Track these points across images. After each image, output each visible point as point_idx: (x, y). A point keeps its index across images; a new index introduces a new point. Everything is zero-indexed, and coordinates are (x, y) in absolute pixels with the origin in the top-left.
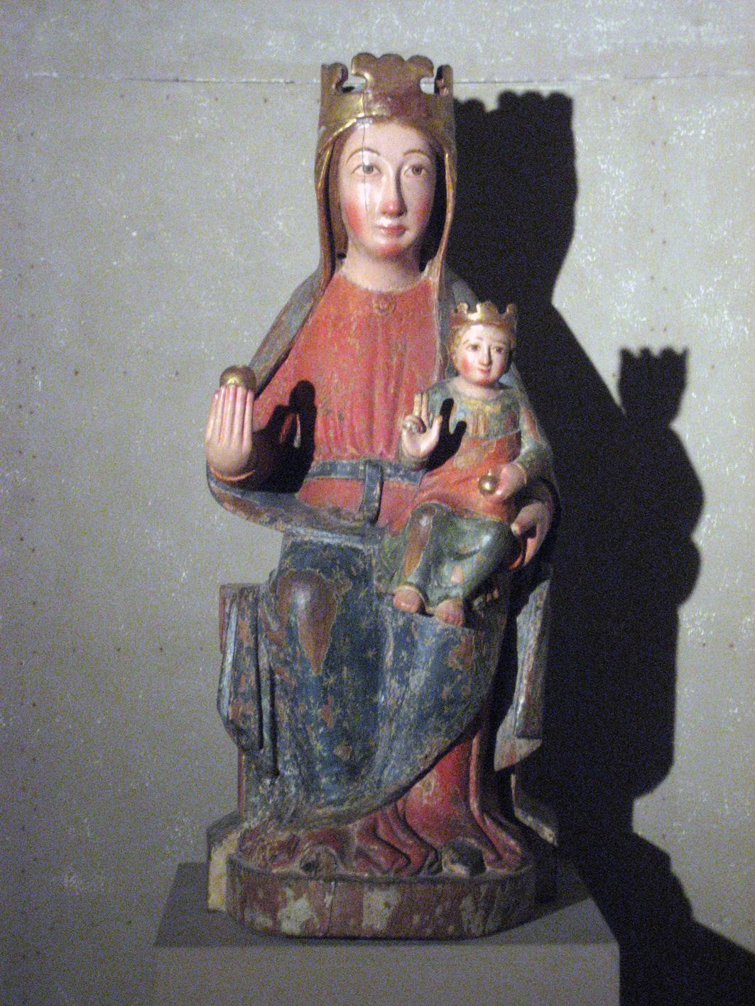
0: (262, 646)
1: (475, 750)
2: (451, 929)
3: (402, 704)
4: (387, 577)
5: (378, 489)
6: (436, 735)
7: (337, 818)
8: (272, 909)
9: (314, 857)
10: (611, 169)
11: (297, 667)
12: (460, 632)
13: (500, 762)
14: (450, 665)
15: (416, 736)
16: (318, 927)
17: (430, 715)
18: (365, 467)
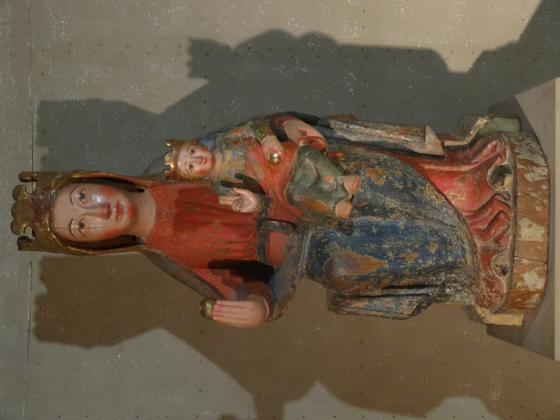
0: (368, 293)
1: (432, 167)
2: (544, 187)
3: (405, 212)
4: (329, 220)
5: (274, 222)
6: (425, 192)
7: (474, 253)
8: (528, 294)
9: (498, 268)
10: (85, 76)
11: (382, 275)
12: (363, 177)
13: (439, 151)
14: (383, 183)
15: (425, 204)
16: (542, 268)
17: (413, 196)
18: (262, 229)
